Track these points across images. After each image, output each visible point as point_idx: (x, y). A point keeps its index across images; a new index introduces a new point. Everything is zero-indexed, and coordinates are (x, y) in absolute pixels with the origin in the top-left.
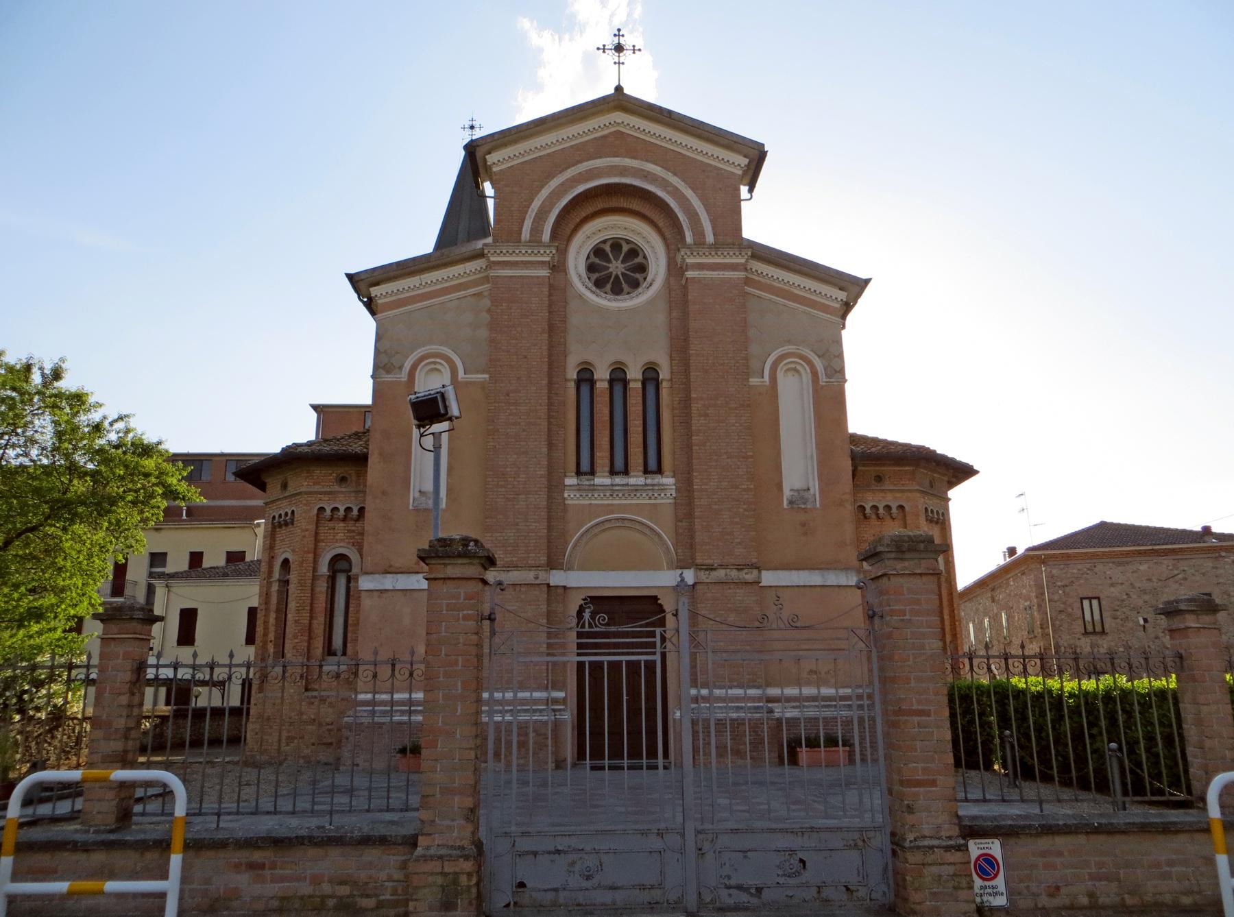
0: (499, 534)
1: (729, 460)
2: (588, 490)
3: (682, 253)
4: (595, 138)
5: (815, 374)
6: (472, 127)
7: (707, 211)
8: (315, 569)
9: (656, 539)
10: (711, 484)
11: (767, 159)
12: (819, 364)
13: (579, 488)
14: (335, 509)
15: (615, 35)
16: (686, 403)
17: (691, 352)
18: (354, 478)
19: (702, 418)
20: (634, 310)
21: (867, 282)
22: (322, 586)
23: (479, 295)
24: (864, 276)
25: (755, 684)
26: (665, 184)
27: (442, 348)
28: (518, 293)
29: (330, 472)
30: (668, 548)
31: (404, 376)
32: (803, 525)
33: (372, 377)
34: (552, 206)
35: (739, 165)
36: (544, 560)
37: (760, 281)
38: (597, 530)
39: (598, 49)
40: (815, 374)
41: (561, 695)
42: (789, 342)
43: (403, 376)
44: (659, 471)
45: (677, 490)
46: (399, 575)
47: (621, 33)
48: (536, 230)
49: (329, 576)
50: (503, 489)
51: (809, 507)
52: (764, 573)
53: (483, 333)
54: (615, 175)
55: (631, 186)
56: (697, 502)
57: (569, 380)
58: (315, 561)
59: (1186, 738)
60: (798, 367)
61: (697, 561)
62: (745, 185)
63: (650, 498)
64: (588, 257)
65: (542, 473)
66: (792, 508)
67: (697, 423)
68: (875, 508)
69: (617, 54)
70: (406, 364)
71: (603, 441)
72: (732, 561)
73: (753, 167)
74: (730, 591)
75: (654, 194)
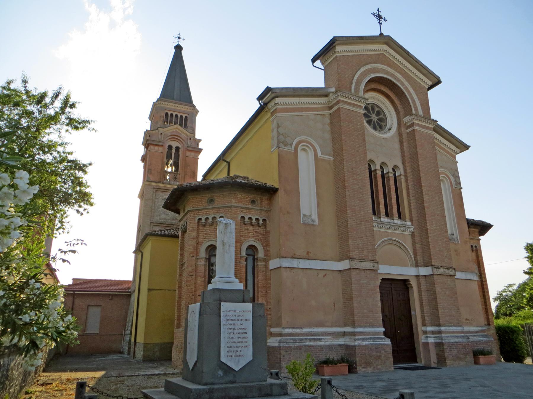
0: (355, 242)
4: (375, 54)
6: (179, 38)
18: (259, 202)
20: (381, 138)
23: (323, 115)
24: (469, 145)
28: (352, 118)
35: (428, 84)
46: (300, 260)
54: (384, 74)
59: (499, 349)
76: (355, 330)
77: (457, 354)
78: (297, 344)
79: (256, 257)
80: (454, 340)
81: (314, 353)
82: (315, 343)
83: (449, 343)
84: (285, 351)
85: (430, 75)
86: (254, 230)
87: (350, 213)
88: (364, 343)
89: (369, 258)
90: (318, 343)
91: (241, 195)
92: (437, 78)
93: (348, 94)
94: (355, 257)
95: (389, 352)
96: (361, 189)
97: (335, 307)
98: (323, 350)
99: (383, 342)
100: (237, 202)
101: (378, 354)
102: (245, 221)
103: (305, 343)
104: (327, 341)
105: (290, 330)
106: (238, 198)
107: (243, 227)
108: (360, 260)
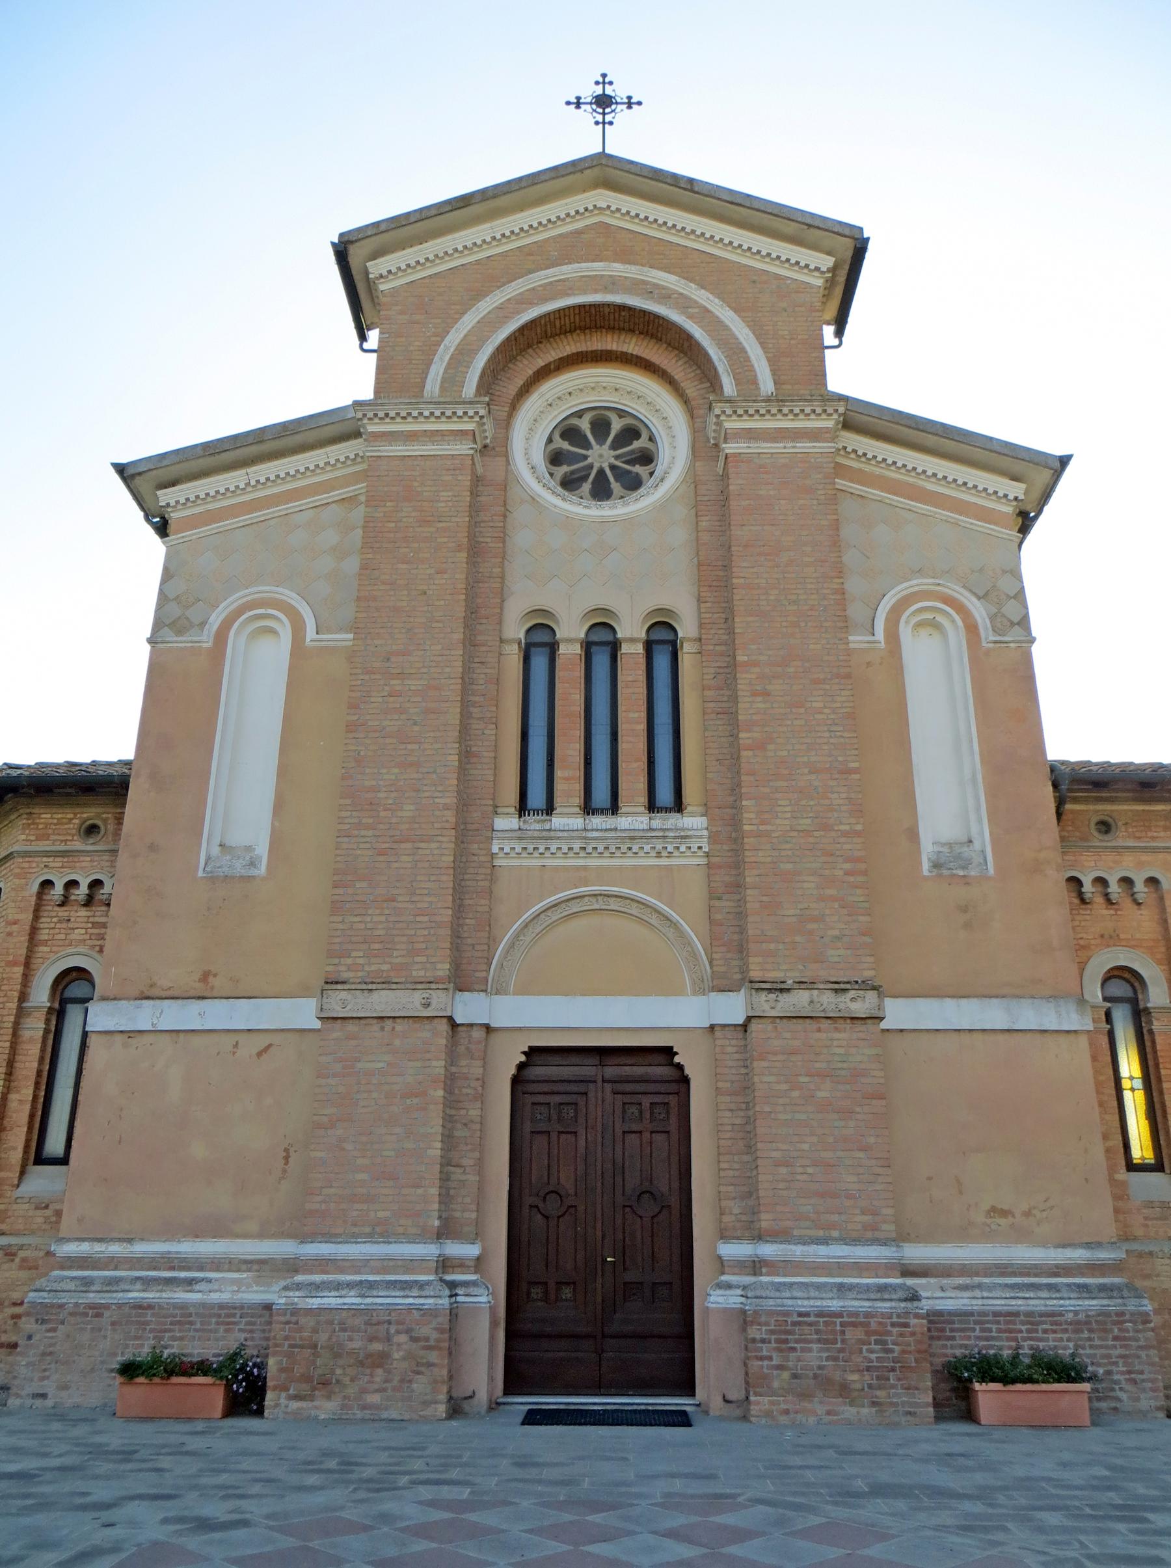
1: (813, 777)
2: (541, 838)
3: (717, 411)
5: (972, 629)
7: (763, 345)
8: (23, 997)
9: (671, 932)
10: (778, 821)
11: (868, 255)
12: (979, 611)
13: (520, 835)
14: (72, 884)
15: (597, 83)
16: (729, 672)
17: (735, 581)
19: (759, 699)
21: (1064, 461)
22: (35, 1028)
25: (877, 1234)
26: (684, 304)
27: (279, 589)
28: (416, 484)
29: (69, 816)
30: (694, 955)
31: (206, 639)
32: (964, 909)
33: (150, 641)
34: (483, 340)
36: (443, 969)
37: (860, 470)
38: (555, 915)
39: (568, 103)
40: (972, 629)
41: (473, 1250)
42: (920, 572)
43: (204, 638)
44: (678, 806)
45: (713, 838)
47: (607, 80)
48: (452, 380)
49: (50, 1010)
50: (370, 833)
51: (973, 873)
52: (888, 1002)
53: (352, 565)
54: (596, 291)
55: (623, 308)
56: (750, 856)
57: (508, 641)
58: (26, 978)
60: (940, 618)
61: (752, 974)
62: (829, 324)
63: (659, 855)
64: (550, 440)
65: (448, 801)
66: (940, 876)
67: (748, 707)
68: (1101, 881)
69: (600, 110)
70: (211, 620)
71: (570, 750)
72: (823, 974)
73: (842, 278)
74: (818, 1035)
75: (657, 317)
76: (759, 1252)
77: (820, 1367)
78: (92, 1297)
79: (1141, 1006)
80: (819, 1303)
81: (151, 1331)
82: (164, 1295)
83: (779, 1313)
84: (37, 1321)
85: (812, 230)
86: (91, 920)
87: (351, 817)
88: (314, 1303)
89: (414, 973)
90: (176, 1295)
91: (49, 816)
92: (847, 232)
93: (396, 404)
94: (345, 976)
95: (432, 1343)
96: (415, 724)
97: (287, 1163)
98: (191, 1323)
99: (411, 1301)
100: (33, 838)
101: (377, 1347)
102: (1135, 890)
103: (121, 1295)
104: (216, 1287)
105: (84, 1248)
106: (37, 824)
107: (54, 914)
108: (364, 986)
